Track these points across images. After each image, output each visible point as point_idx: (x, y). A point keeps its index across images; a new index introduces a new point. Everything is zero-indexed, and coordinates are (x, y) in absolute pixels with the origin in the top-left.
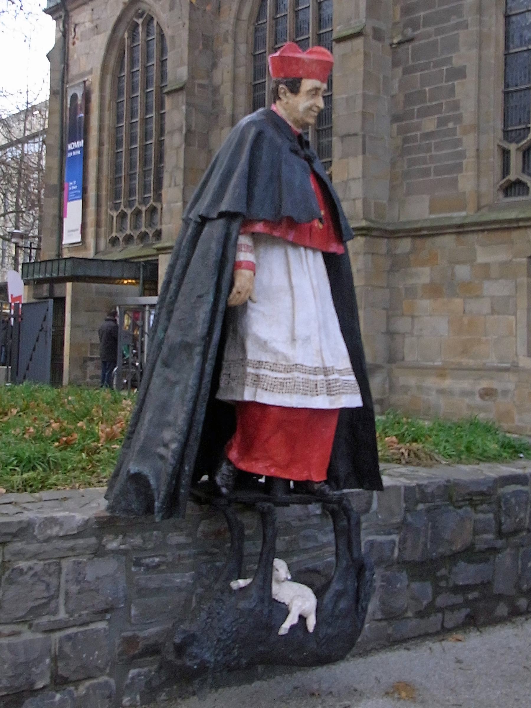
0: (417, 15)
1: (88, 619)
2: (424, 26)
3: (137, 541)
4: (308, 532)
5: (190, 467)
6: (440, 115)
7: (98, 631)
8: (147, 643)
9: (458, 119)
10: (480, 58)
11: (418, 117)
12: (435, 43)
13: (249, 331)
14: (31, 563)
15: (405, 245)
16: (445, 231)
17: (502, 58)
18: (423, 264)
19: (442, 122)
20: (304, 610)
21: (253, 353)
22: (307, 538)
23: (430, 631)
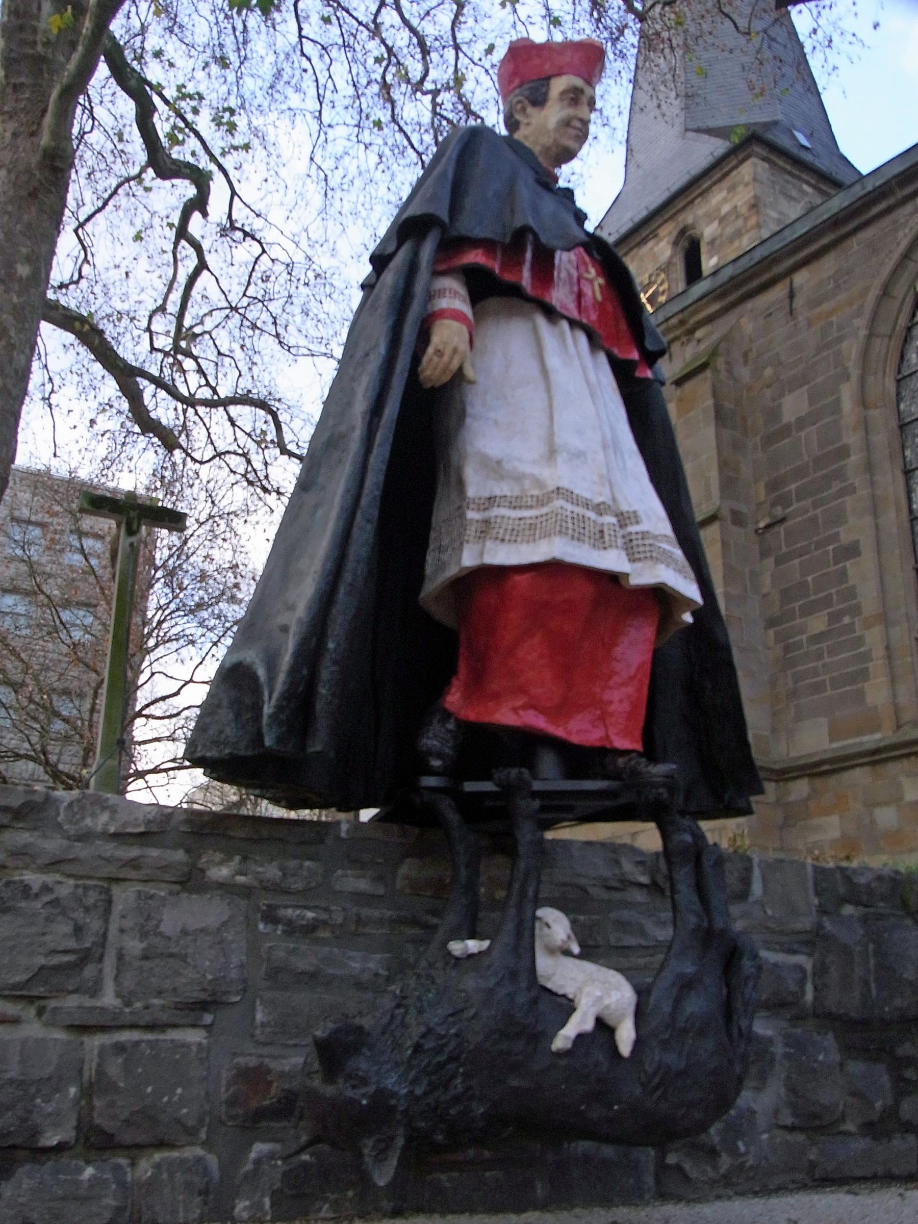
0: (787, 489)
1: (164, 1017)
2: (798, 500)
3: (272, 872)
4: (626, 915)
5: (339, 644)
6: (830, 610)
7: (186, 1046)
8: (287, 1086)
9: (856, 611)
10: (877, 527)
11: (801, 617)
12: (814, 519)
13: (470, 449)
14: (50, 878)
15: (800, 788)
16: (855, 762)
17: (907, 525)
18: (827, 812)
19: (835, 617)
20: (608, 1007)
21: (476, 485)
22: (622, 925)
23: (896, 1171)
